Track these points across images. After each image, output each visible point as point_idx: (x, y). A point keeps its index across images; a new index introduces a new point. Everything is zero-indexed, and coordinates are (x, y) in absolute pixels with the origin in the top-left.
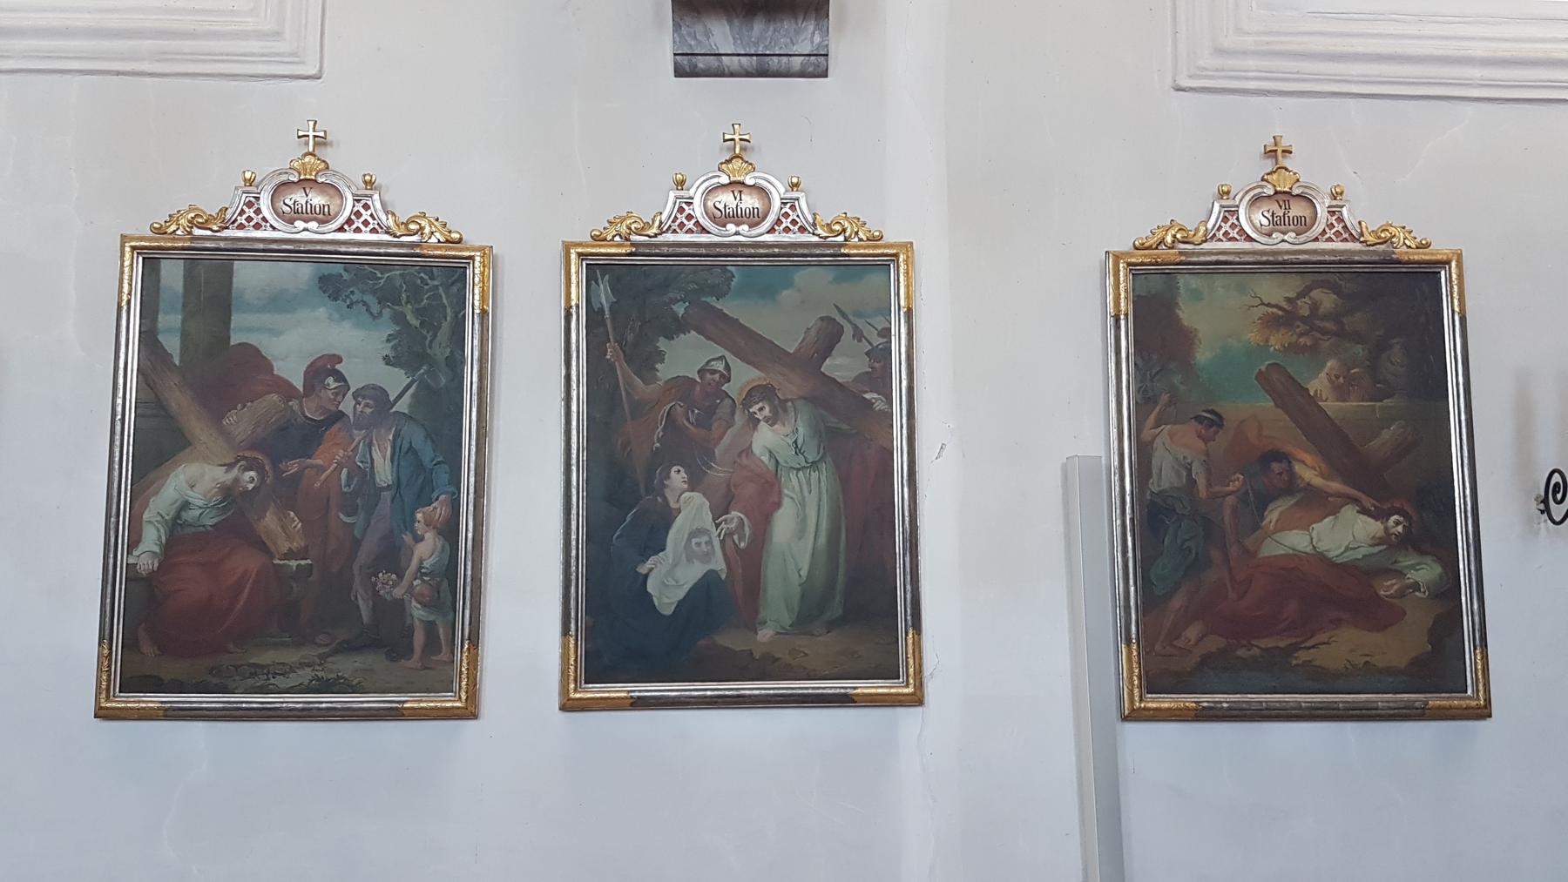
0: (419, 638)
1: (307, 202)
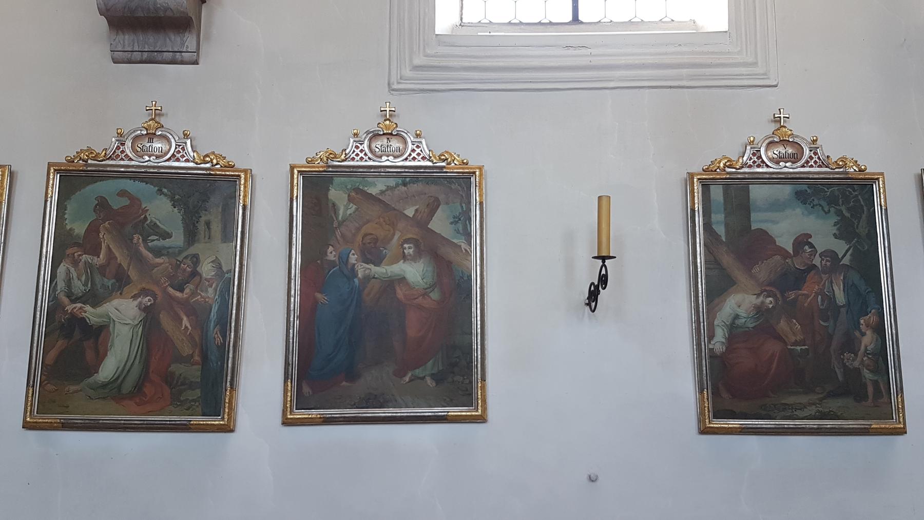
0: (870, 389)
1: (388, 146)
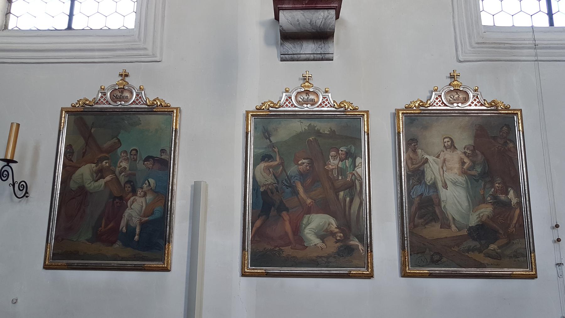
1: (458, 96)
